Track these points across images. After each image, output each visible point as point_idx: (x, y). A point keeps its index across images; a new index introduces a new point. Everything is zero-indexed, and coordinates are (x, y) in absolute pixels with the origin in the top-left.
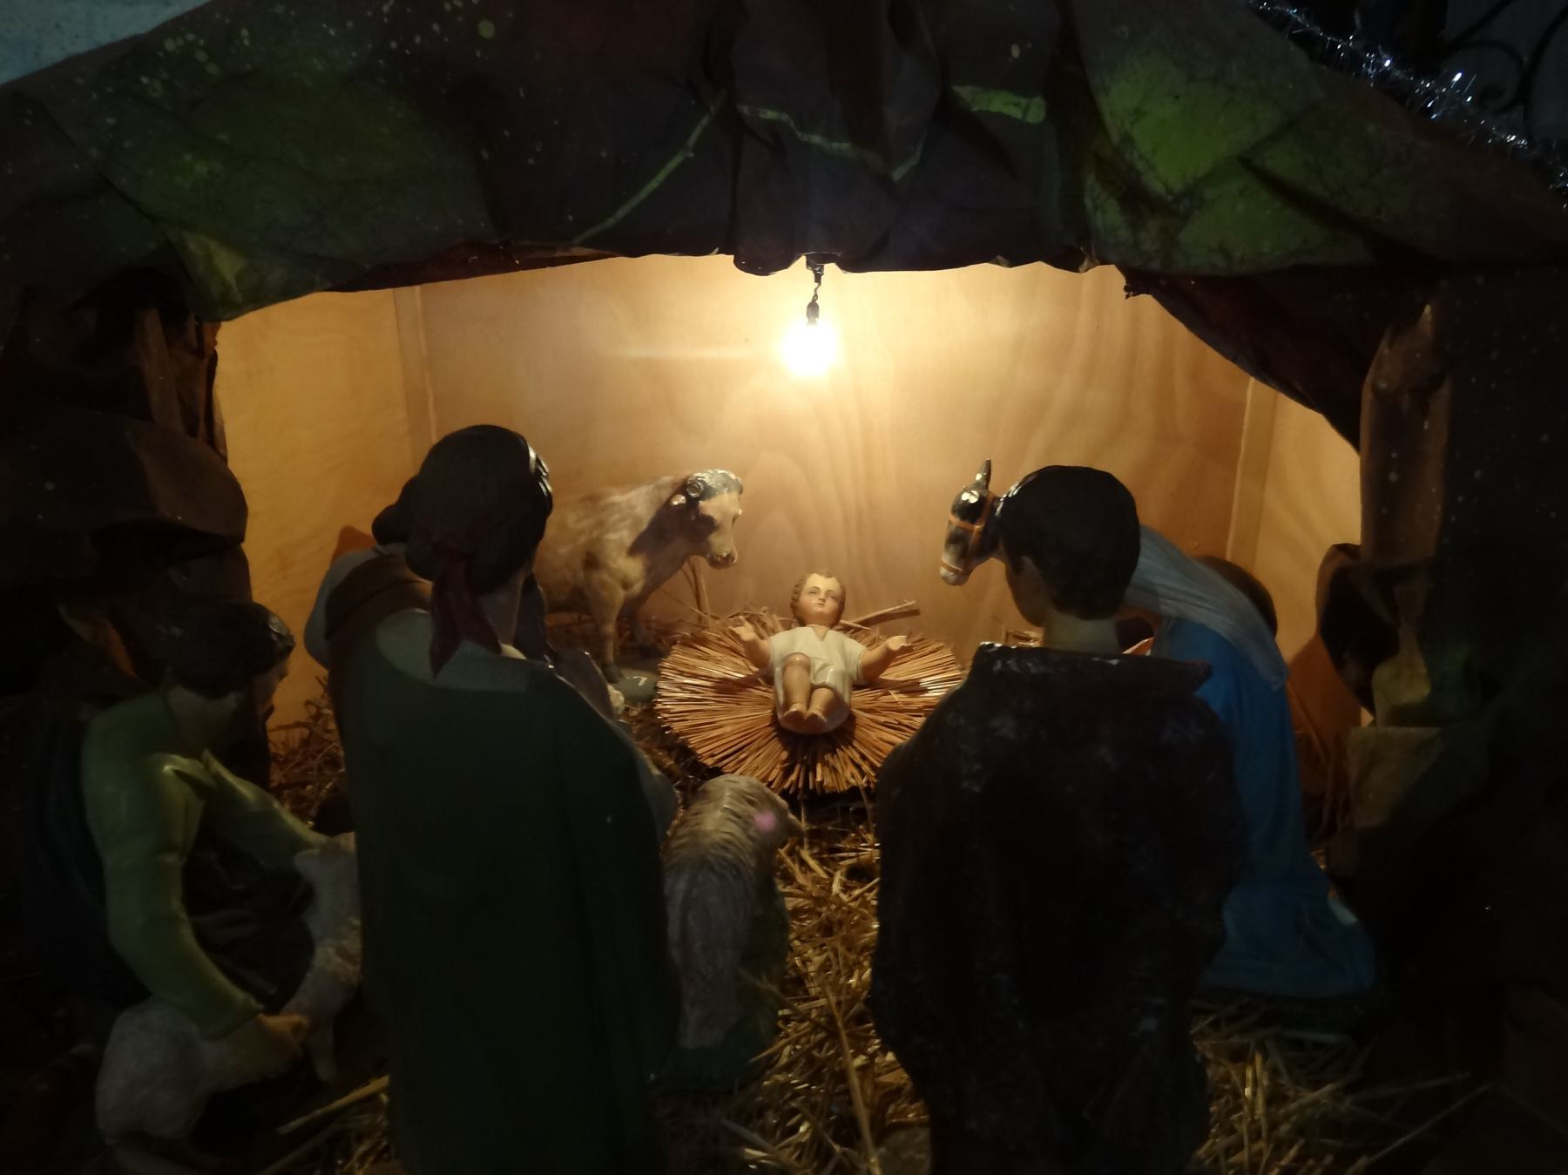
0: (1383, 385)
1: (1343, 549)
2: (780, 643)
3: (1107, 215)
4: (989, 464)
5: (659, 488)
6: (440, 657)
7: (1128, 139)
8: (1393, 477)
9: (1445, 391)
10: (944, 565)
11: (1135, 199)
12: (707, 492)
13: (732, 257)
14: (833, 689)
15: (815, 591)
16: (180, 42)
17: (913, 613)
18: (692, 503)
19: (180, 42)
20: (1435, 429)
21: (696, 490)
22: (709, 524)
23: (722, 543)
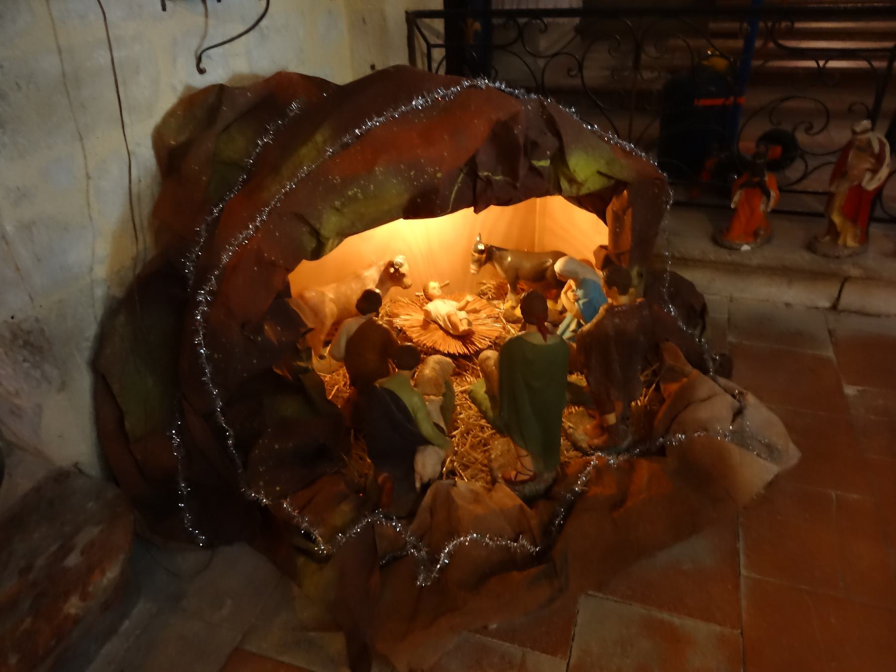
0: (615, 209)
1: (602, 247)
2: (431, 307)
3: (564, 184)
4: (480, 234)
5: (379, 267)
6: (545, 338)
7: (575, 171)
8: (618, 230)
9: (630, 210)
10: (473, 269)
11: (572, 181)
12: (401, 265)
13: (472, 209)
14: (466, 318)
15: (434, 288)
16: (353, 192)
17: (447, 284)
18: (397, 270)
19: (353, 192)
20: (628, 219)
21: (397, 265)
22: (403, 275)
23: (407, 281)
